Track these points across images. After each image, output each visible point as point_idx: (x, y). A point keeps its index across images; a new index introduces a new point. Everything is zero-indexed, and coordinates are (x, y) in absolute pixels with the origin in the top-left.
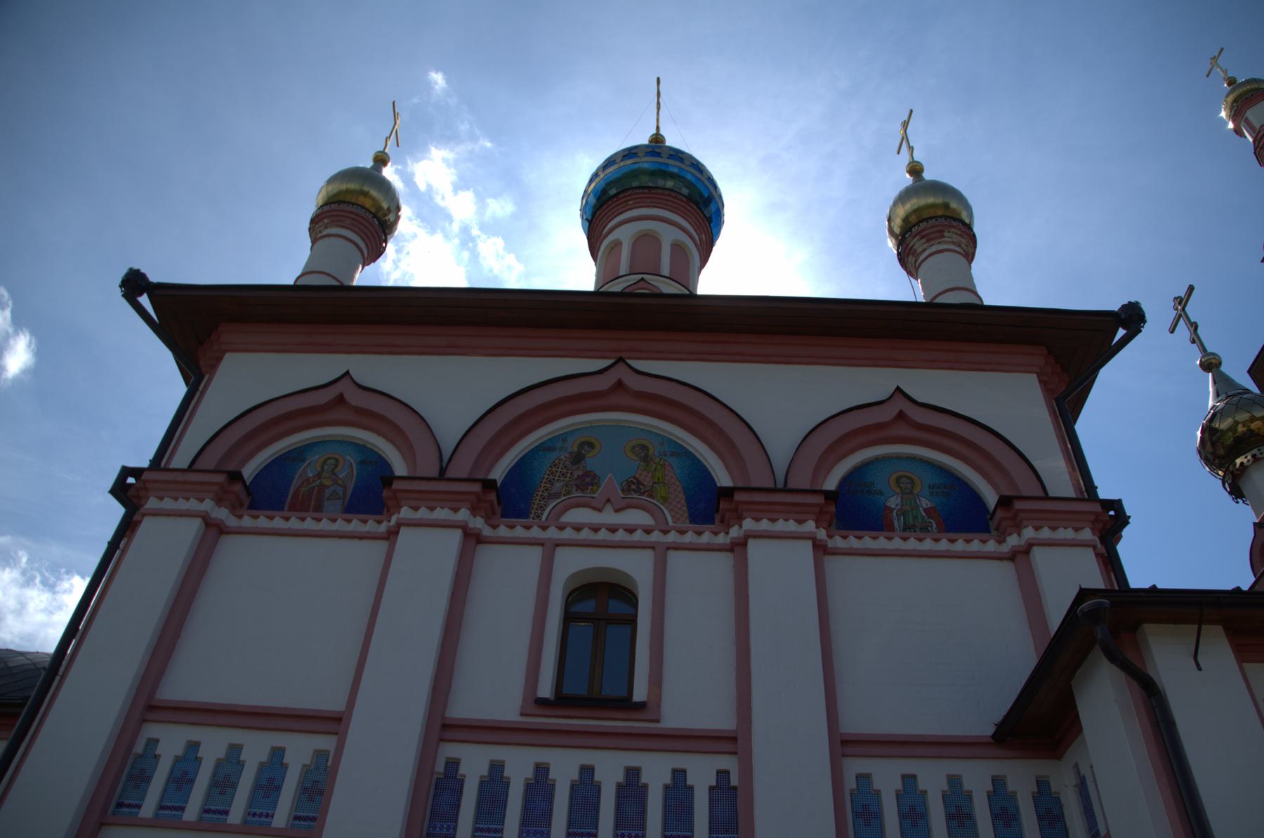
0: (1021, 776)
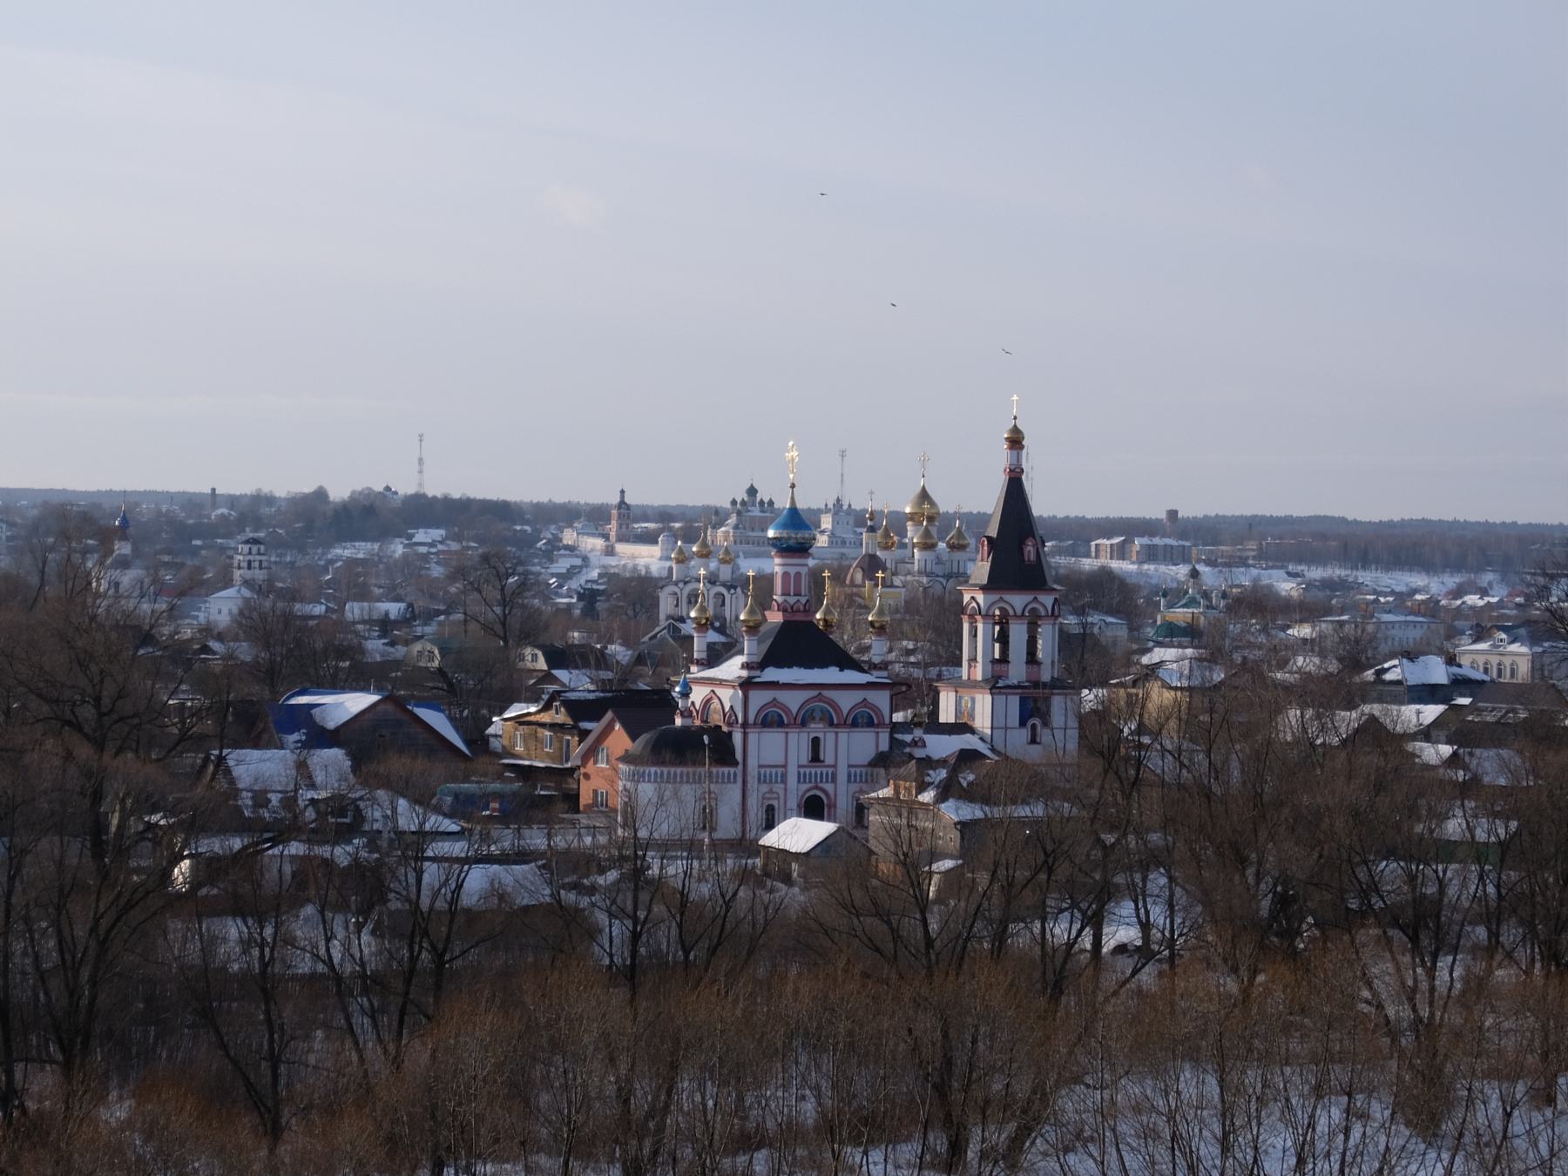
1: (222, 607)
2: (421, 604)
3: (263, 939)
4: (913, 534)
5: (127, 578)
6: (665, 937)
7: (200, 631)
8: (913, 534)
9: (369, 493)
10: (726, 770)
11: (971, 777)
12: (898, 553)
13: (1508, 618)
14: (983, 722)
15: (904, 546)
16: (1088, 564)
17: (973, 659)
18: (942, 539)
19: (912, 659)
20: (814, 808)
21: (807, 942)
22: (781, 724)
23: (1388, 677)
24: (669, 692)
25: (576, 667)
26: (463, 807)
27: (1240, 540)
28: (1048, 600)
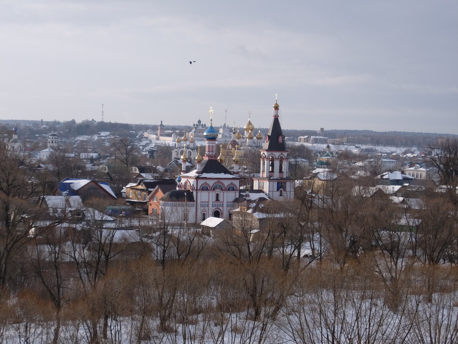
1: (44, 154)
2: (102, 154)
3: (55, 251)
4: (246, 134)
5: (16, 146)
6: (173, 252)
7: (38, 161)
8: (246, 134)
9: (87, 121)
10: (191, 203)
11: (263, 206)
12: (242, 140)
13: (420, 160)
14: (266, 189)
15: (244, 138)
16: (297, 144)
17: (264, 171)
18: (255, 136)
19: (246, 171)
20: (217, 214)
21: (215, 253)
22: (207, 190)
23: (384, 177)
24: (175, 180)
25: (148, 173)
26: (114, 213)
27: (341, 137)
28: (285, 154)
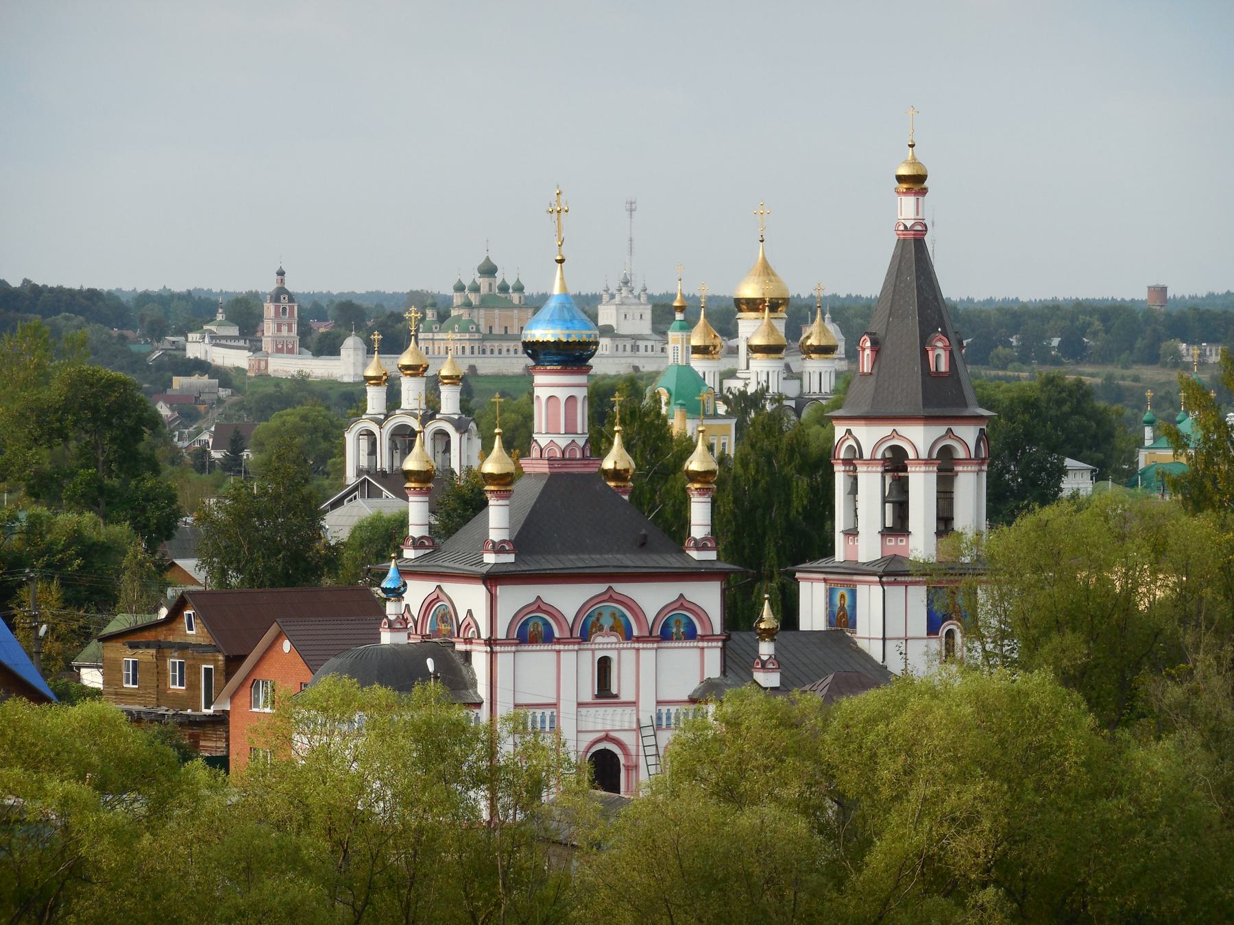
0: (692, 707)
17: (852, 533)
22: (548, 638)
